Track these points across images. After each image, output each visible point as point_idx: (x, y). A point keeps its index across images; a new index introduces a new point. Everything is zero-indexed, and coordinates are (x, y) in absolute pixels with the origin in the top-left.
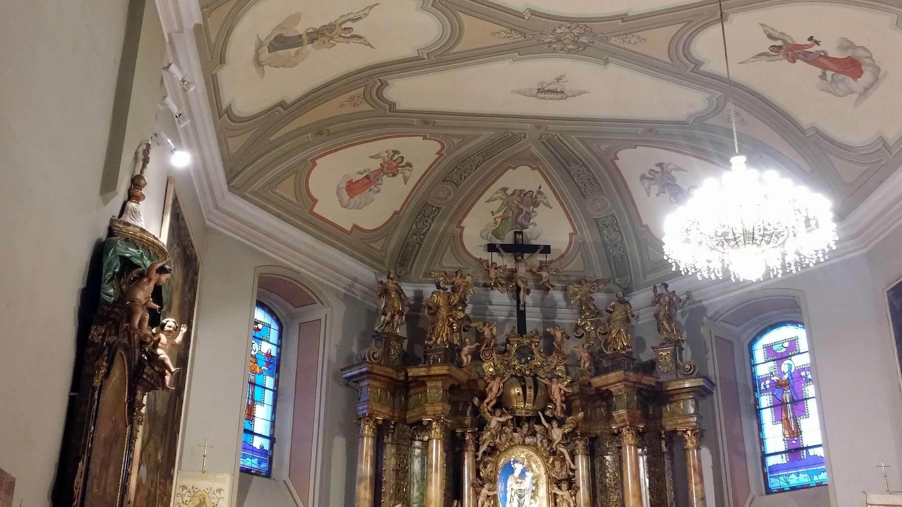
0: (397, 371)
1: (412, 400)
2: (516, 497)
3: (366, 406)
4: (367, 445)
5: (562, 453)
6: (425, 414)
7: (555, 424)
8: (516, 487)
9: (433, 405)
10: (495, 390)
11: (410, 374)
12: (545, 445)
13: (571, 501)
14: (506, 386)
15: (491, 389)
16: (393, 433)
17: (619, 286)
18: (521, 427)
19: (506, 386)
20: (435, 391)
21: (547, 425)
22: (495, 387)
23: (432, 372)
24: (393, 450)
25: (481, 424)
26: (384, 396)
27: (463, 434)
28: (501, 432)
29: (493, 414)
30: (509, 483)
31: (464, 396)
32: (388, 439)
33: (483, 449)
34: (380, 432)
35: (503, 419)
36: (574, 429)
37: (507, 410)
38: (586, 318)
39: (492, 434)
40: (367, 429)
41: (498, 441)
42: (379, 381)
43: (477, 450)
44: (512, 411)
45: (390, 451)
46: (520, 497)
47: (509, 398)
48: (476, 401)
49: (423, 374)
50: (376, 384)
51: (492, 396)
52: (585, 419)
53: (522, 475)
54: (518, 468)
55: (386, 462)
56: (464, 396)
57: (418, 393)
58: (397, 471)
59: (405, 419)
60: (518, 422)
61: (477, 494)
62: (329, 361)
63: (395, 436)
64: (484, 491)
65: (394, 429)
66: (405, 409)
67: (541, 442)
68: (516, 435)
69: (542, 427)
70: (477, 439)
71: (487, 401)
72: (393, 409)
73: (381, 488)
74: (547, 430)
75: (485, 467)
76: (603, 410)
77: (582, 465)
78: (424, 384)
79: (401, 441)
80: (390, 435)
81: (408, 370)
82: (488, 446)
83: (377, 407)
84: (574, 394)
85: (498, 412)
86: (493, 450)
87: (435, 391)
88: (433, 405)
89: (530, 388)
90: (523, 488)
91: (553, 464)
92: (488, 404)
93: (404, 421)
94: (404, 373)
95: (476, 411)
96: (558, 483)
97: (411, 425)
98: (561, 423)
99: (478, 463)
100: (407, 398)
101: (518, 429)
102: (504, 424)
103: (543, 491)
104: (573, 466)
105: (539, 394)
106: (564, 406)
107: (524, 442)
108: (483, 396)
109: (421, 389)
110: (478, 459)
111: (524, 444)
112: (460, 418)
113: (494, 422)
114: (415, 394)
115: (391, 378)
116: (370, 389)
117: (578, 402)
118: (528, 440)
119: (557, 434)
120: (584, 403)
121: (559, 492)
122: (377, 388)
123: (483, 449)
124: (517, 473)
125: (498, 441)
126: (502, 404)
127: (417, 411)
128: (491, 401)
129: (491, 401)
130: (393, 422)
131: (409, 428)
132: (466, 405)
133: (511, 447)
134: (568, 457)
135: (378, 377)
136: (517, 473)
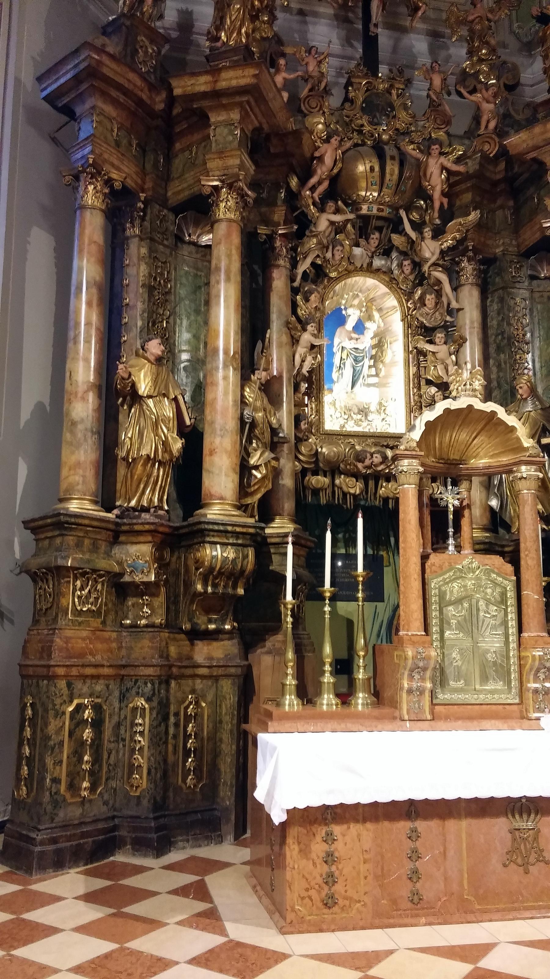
0: (152, 87)
1: (178, 163)
2: (349, 362)
3: (88, 149)
4: (92, 227)
5: (439, 282)
6: (207, 173)
7: (428, 232)
8: (349, 345)
9: (221, 161)
10: (328, 160)
11: (177, 92)
12: (407, 269)
13: (449, 362)
14: (346, 159)
15: (321, 159)
16: (143, 219)
17: (518, 37)
18: (367, 239)
19: (346, 159)
20: (226, 127)
21: (413, 235)
22: (329, 154)
23: (223, 84)
24: (144, 251)
25: (303, 225)
26: (125, 142)
27: (271, 238)
28: (334, 243)
29: (322, 210)
30: (336, 341)
31: (277, 156)
32: (133, 231)
33: (304, 266)
34: (119, 207)
35: (337, 218)
36: (460, 242)
37: (347, 205)
38: (481, 61)
39: (319, 243)
40: (91, 195)
41: (329, 255)
42: (115, 102)
43: (294, 264)
44: (354, 206)
45: (136, 250)
46: (356, 360)
47: (353, 182)
48: (294, 182)
49: (203, 88)
50: (109, 109)
51: (321, 172)
52: (479, 226)
53: (359, 328)
54: (353, 316)
55: (131, 271)
56: (277, 156)
57: (189, 148)
58: (151, 289)
59: (166, 200)
60: (364, 227)
61: (295, 341)
62: (17, 80)
63: (147, 224)
64: (306, 338)
65: (144, 210)
66: (166, 178)
67: (400, 266)
68: (357, 251)
69: (403, 239)
70: (294, 249)
71: (314, 180)
72: (143, 173)
73: (120, 316)
74: (412, 243)
75: (307, 300)
76: (508, 213)
77: (469, 302)
78: (203, 120)
79: (158, 237)
80: (137, 222)
81: (174, 83)
82: (313, 264)
83: (110, 155)
84: (467, 177)
85: (331, 205)
86: (318, 274)
87: (226, 127)
88: (221, 161)
89: (393, 158)
90: (361, 347)
91: (422, 300)
92: (313, 189)
93: (164, 203)
94: (164, 95)
95: (293, 198)
96: (428, 333)
97: (177, 210)
98: (438, 233)
99: (295, 291)
100: (168, 159)
101: (362, 242)
102: (338, 228)
103: (396, 351)
104: (454, 305)
105: (407, 174)
106: (445, 201)
107: (370, 264)
108: (305, 174)
109: (197, 137)
110: (296, 284)
111: (369, 270)
112: (264, 209)
113: (323, 224)
114: (183, 150)
115: (140, 102)
116: (96, 123)
117: (467, 197)
118: (378, 262)
119: (430, 249)
120: (478, 199)
121: (429, 347)
122: (110, 119)
123: (304, 266)
124: (350, 324)
125: (329, 255)
126: (339, 190)
127: (189, 177)
128: (320, 183)
129: (320, 183)
130: (142, 196)
131: (171, 216)
132: (277, 187)
133: (348, 273)
134: (447, 288)
135: (114, 93)
136: (350, 324)
